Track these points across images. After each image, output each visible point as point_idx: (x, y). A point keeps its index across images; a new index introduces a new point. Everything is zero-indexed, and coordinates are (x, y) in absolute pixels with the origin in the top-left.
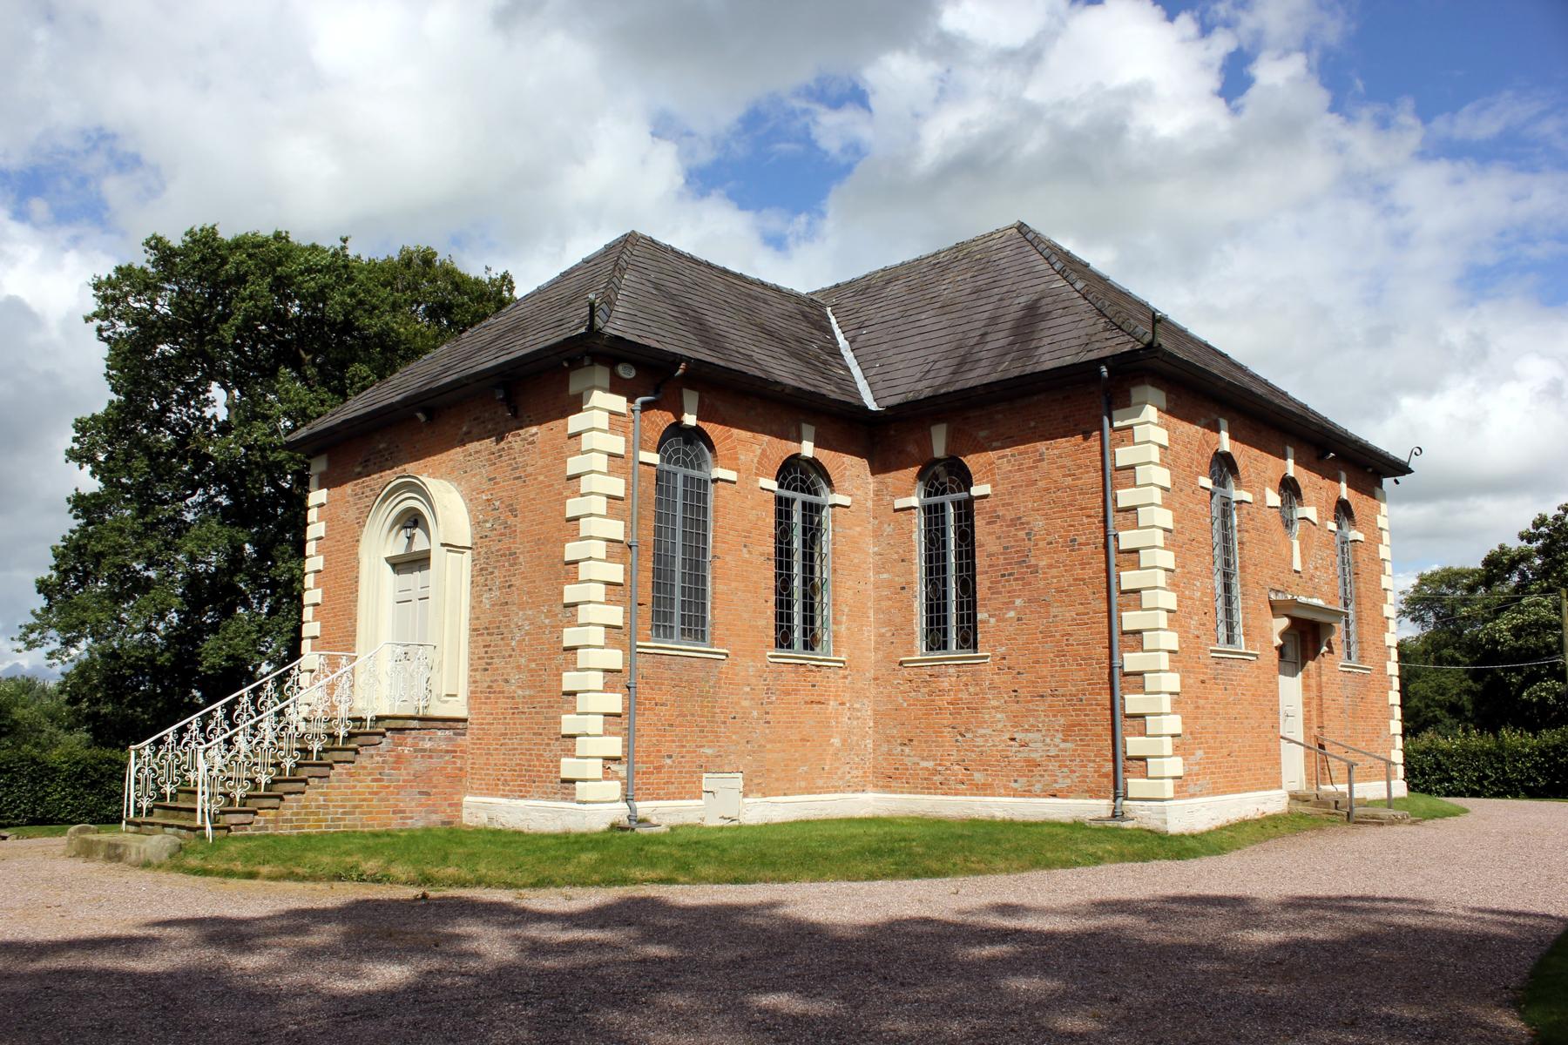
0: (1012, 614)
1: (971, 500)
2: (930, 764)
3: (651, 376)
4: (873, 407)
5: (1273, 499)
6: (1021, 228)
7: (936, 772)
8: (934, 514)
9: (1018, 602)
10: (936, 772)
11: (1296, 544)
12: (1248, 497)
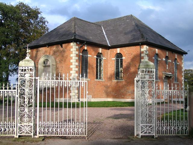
0: (127, 75)
1: (122, 59)
2: (116, 95)
3: (81, 42)
4: (109, 45)
5: (164, 59)
6: (131, 15)
7: (117, 96)
8: (97, 59)
9: (128, 73)
10: (117, 96)
11: (167, 65)
12: (160, 59)
